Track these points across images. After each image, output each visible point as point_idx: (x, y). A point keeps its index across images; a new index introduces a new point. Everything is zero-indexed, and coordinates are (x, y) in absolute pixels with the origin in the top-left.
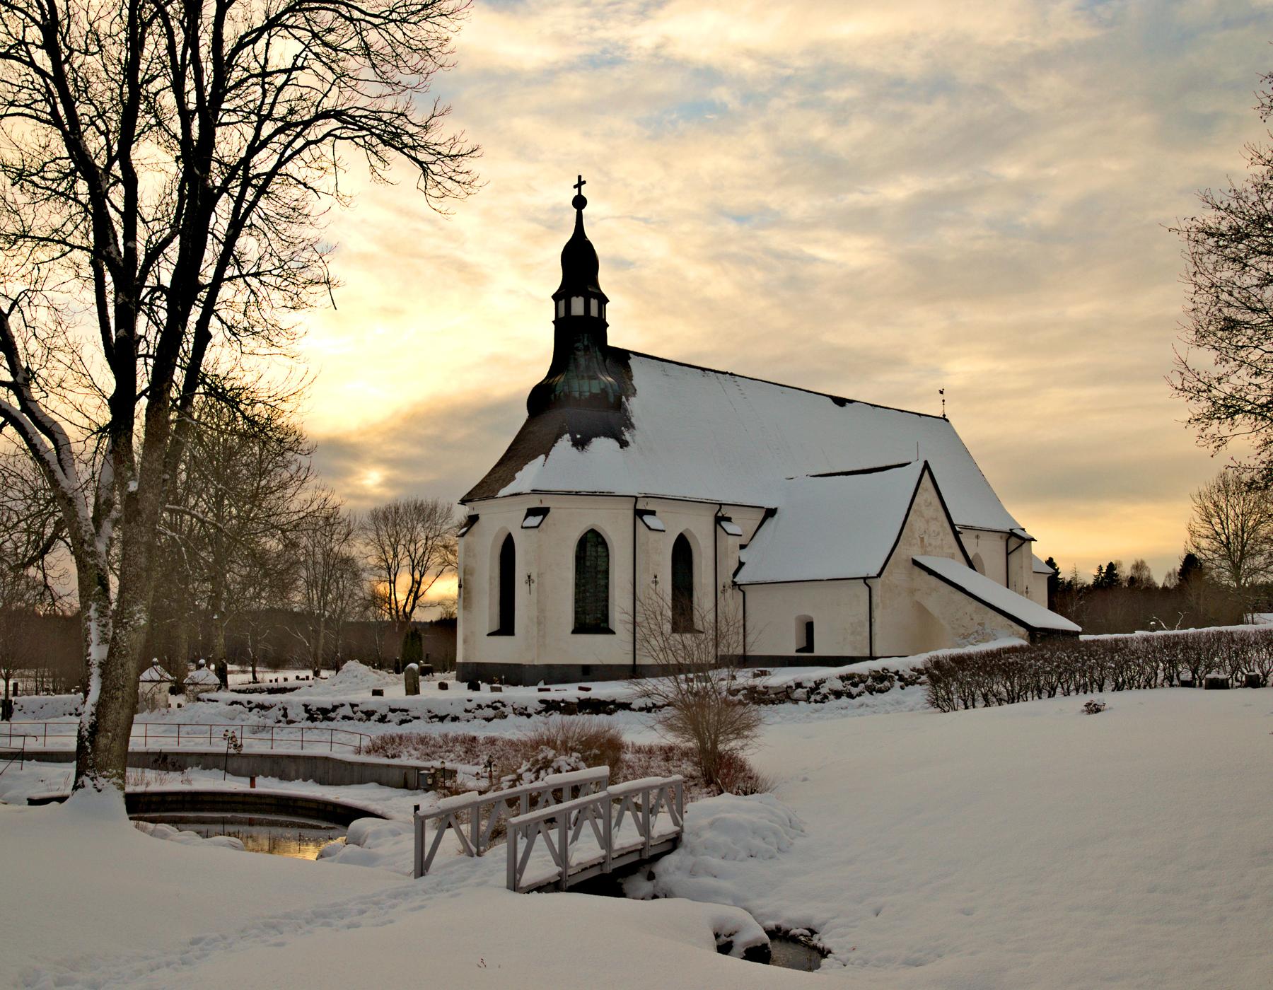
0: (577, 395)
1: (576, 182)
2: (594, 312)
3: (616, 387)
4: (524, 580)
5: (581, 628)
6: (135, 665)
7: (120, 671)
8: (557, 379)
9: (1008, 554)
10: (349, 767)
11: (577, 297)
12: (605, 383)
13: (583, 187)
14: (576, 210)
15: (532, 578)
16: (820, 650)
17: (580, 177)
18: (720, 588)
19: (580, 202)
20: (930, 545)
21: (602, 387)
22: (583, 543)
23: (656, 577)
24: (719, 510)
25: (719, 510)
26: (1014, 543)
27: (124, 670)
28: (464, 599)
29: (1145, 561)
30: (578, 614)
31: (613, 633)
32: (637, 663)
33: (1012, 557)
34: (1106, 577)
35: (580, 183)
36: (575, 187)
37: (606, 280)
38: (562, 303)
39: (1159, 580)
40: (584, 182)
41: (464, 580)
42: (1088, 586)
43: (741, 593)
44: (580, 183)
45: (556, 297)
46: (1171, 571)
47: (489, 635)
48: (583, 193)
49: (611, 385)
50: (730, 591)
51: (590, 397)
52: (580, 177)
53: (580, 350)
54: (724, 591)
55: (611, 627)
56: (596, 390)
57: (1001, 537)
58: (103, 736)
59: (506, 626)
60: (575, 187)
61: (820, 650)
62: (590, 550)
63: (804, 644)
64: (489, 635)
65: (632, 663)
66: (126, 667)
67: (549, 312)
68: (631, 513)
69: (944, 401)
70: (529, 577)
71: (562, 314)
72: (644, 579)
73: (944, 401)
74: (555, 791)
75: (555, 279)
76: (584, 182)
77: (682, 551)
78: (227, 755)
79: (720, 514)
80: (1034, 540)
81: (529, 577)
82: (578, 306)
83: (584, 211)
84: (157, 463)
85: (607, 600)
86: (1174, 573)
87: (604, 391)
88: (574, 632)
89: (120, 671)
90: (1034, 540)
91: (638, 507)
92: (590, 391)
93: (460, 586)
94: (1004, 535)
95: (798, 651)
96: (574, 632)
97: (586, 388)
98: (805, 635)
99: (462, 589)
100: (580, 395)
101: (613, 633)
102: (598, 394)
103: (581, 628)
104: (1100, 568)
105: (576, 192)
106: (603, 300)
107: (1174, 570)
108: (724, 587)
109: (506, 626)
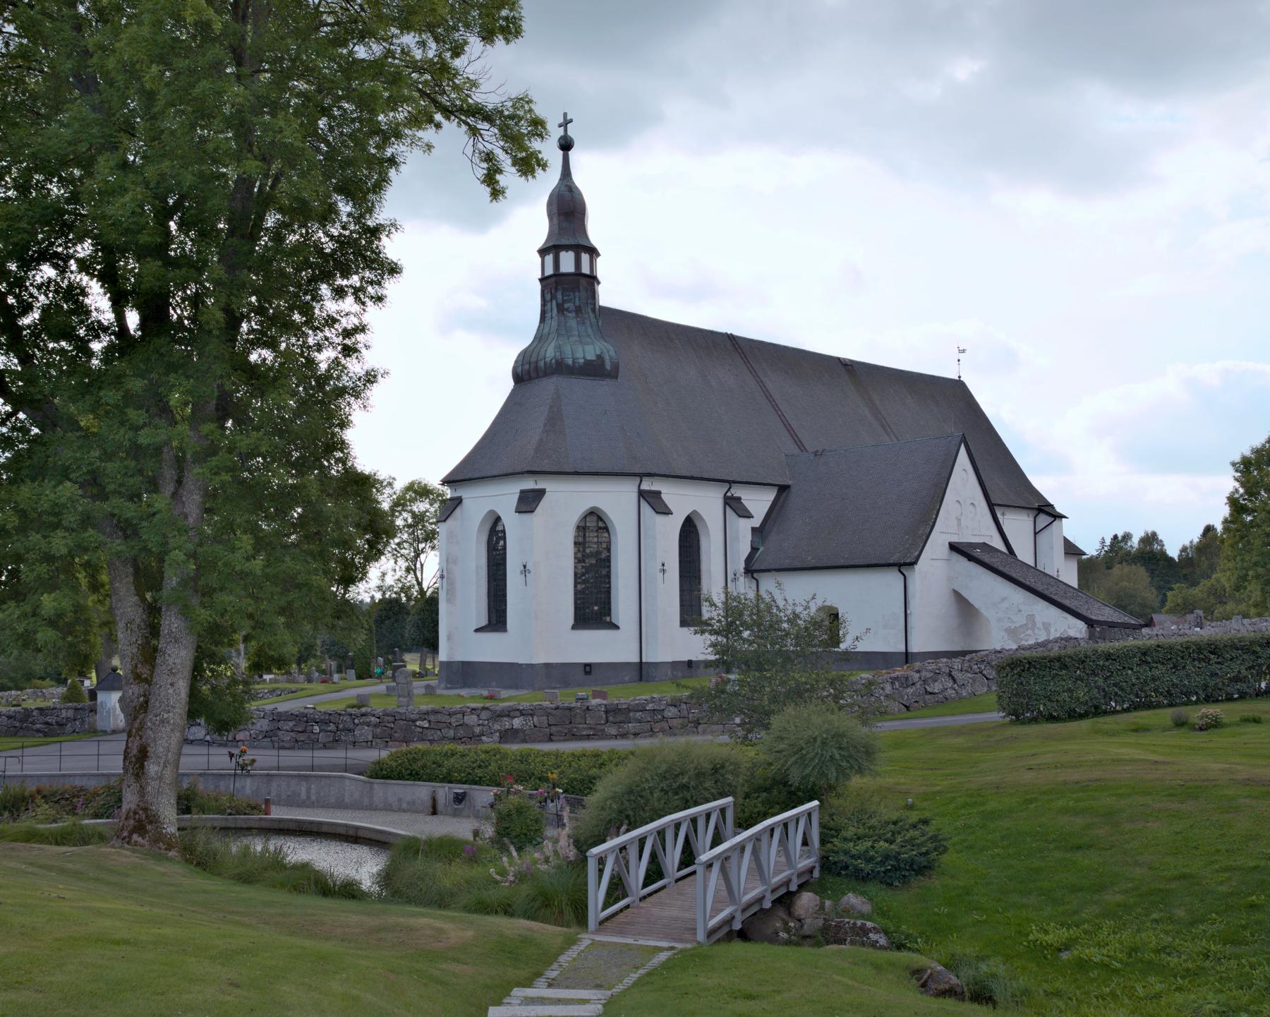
0: (570, 362)
1: (561, 120)
3: (612, 353)
4: (518, 571)
6: (185, 685)
7: (171, 691)
9: (1036, 534)
17: (565, 115)
20: (967, 527)
21: (598, 353)
22: (582, 529)
23: (663, 565)
27: (174, 691)
29: (1158, 533)
30: (578, 609)
31: (616, 627)
32: (644, 660)
33: (1041, 537)
34: (1111, 551)
36: (560, 126)
37: (596, 231)
38: (549, 259)
39: (1173, 552)
40: (571, 121)
41: (447, 569)
43: (755, 581)
45: (543, 252)
46: (1187, 544)
47: (477, 630)
48: (570, 133)
50: (742, 579)
51: (584, 363)
52: (565, 115)
53: (570, 312)
54: (735, 579)
58: (153, 763)
59: (497, 619)
60: (560, 126)
62: (592, 537)
64: (477, 630)
65: (637, 660)
66: (176, 686)
68: (635, 496)
69: (959, 360)
70: (525, 566)
72: (650, 567)
73: (959, 360)
74: (676, 824)
77: (690, 533)
79: (729, 494)
80: (1065, 517)
81: (525, 566)
82: (567, 262)
83: (570, 153)
85: (609, 592)
86: (1191, 547)
88: (574, 628)
89: (171, 691)
90: (1065, 517)
91: (642, 487)
92: (584, 358)
96: (574, 628)
100: (574, 362)
101: (616, 627)
102: (594, 361)
104: (1103, 541)
105: (561, 132)
107: (1191, 542)
108: (735, 575)
109: (497, 619)
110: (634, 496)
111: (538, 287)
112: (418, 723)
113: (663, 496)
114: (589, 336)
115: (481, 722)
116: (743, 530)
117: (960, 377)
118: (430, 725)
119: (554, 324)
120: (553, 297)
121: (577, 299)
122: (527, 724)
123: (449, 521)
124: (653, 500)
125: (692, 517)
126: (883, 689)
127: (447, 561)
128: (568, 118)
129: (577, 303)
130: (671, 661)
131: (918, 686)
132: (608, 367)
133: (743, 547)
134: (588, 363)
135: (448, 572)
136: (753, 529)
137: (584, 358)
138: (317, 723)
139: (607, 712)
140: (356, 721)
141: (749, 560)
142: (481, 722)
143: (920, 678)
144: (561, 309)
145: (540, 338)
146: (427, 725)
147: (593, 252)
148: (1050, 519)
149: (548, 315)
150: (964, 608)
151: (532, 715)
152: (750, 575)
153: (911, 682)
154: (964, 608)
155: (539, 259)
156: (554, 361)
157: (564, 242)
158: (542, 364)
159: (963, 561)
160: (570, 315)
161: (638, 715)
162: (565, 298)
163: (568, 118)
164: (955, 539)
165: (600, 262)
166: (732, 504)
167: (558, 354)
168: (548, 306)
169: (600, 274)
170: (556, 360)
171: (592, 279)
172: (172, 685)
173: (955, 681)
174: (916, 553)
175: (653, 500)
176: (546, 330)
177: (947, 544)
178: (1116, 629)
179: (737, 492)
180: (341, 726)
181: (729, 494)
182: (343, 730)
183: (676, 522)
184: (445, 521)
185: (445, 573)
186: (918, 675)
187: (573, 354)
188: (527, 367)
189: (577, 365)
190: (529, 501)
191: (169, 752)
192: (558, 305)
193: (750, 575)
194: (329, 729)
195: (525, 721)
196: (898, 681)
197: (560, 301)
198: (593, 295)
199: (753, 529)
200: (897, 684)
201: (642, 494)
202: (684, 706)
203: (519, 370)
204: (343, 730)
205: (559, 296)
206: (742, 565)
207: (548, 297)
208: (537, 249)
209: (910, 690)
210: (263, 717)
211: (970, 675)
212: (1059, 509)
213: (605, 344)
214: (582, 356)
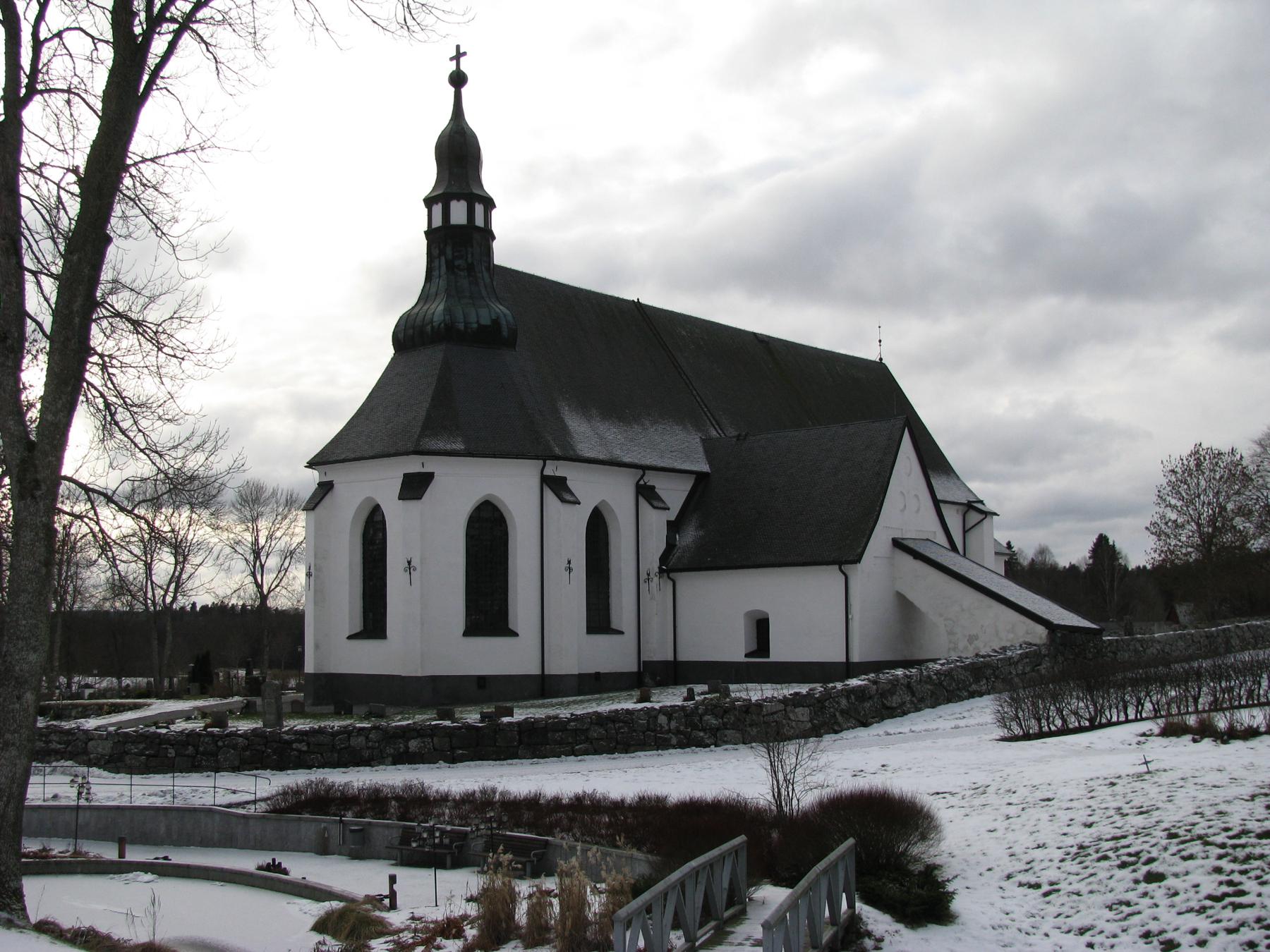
0: (461, 326)
1: (454, 54)
2: (479, 221)
3: (510, 318)
5: (472, 629)
8: (433, 306)
10: (242, 821)
11: (458, 200)
12: (496, 313)
13: (462, 60)
14: (453, 89)
15: (412, 564)
16: (780, 651)
17: (458, 47)
18: (643, 576)
19: (458, 80)
23: (569, 562)
24: (642, 478)
25: (642, 478)
26: (973, 517)
28: (316, 591)
31: (515, 634)
32: (546, 673)
35: (459, 56)
36: (452, 59)
37: (492, 179)
38: (438, 209)
40: (465, 54)
42: (1126, 568)
43: (670, 584)
44: (459, 56)
45: (429, 202)
47: (350, 638)
48: (462, 68)
49: (505, 315)
50: (656, 580)
52: (458, 47)
54: (648, 580)
55: (511, 626)
56: (485, 321)
57: (958, 511)
60: (452, 59)
61: (780, 651)
63: (754, 647)
64: (350, 638)
67: (417, 221)
69: (880, 341)
70: (409, 563)
71: (437, 222)
73: (880, 341)
75: (426, 176)
76: (465, 54)
77: (598, 527)
78: (78, 808)
79: (642, 482)
80: (995, 514)
81: (409, 563)
82: (459, 214)
83: (464, 90)
84: (62, 414)
87: (496, 322)
88: (466, 634)
91: (545, 473)
93: (309, 575)
94: (961, 508)
95: (746, 656)
96: (466, 634)
97: (473, 318)
98: (755, 635)
99: (312, 578)
100: (465, 327)
101: (515, 634)
103: (472, 629)
105: (452, 66)
106: (489, 204)
108: (648, 575)
110: (535, 482)
111: (424, 242)
112: (294, 746)
113: (568, 483)
114: (483, 298)
115: (370, 744)
116: (656, 523)
117: (881, 359)
118: (309, 747)
119: (442, 283)
120: (442, 253)
121: (469, 256)
122: (425, 747)
123: (317, 510)
124: (558, 486)
125: (602, 509)
126: (838, 703)
127: (315, 555)
128: (461, 51)
129: (470, 260)
130: (576, 672)
131: (875, 700)
132: (505, 333)
133: (655, 544)
134: (482, 328)
135: (316, 570)
136: (669, 522)
137: (478, 322)
138: (172, 745)
139: (520, 733)
140: (220, 743)
141: (664, 559)
142: (370, 744)
143: (877, 691)
144: (451, 267)
145: (424, 297)
146: (305, 748)
148: (981, 517)
149: (436, 273)
150: (906, 610)
151: (432, 736)
152: (665, 574)
153: (868, 696)
154: (906, 610)
155: (426, 211)
156: (443, 325)
157: (455, 190)
158: (429, 328)
159: (907, 559)
160: (462, 273)
161: (558, 735)
162: (456, 254)
163: (461, 51)
164: (898, 535)
165: (495, 215)
166: (646, 493)
167: (448, 317)
168: (436, 263)
169: (496, 227)
170: (445, 325)
171: (488, 235)
172: (19, 698)
173: (913, 694)
174: (859, 550)
175: (558, 486)
176: (433, 290)
177: (891, 540)
178: (1076, 634)
179: (652, 479)
180: (201, 749)
181: (642, 482)
182: (203, 754)
183: (584, 512)
184: (313, 509)
185: (312, 570)
186: (875, 687)
187: (465, 317)
188: (411, 331)
189: (469, 330)
190: (414, 487)
191: (14, 783)
192: (447, 262)
193: (665, 574)
194: (187, 752)
195: (424, 742)
196: (854, 694)
197: (450, 256)
198: (488, 252)
199: (669, 522)
200: (853, 697)
201: (546, 481)
202: (611, 725)
203: (401, 336)
204: (203, 754)
205: (449, 251)
206: (656, 564)
207: (436, 252)
208: (424, 197)
209: (867, 705)
210: (106, 739)
211: (929, 687)
212: (990, 505)
213: (501, 307)
214: (476, 320)
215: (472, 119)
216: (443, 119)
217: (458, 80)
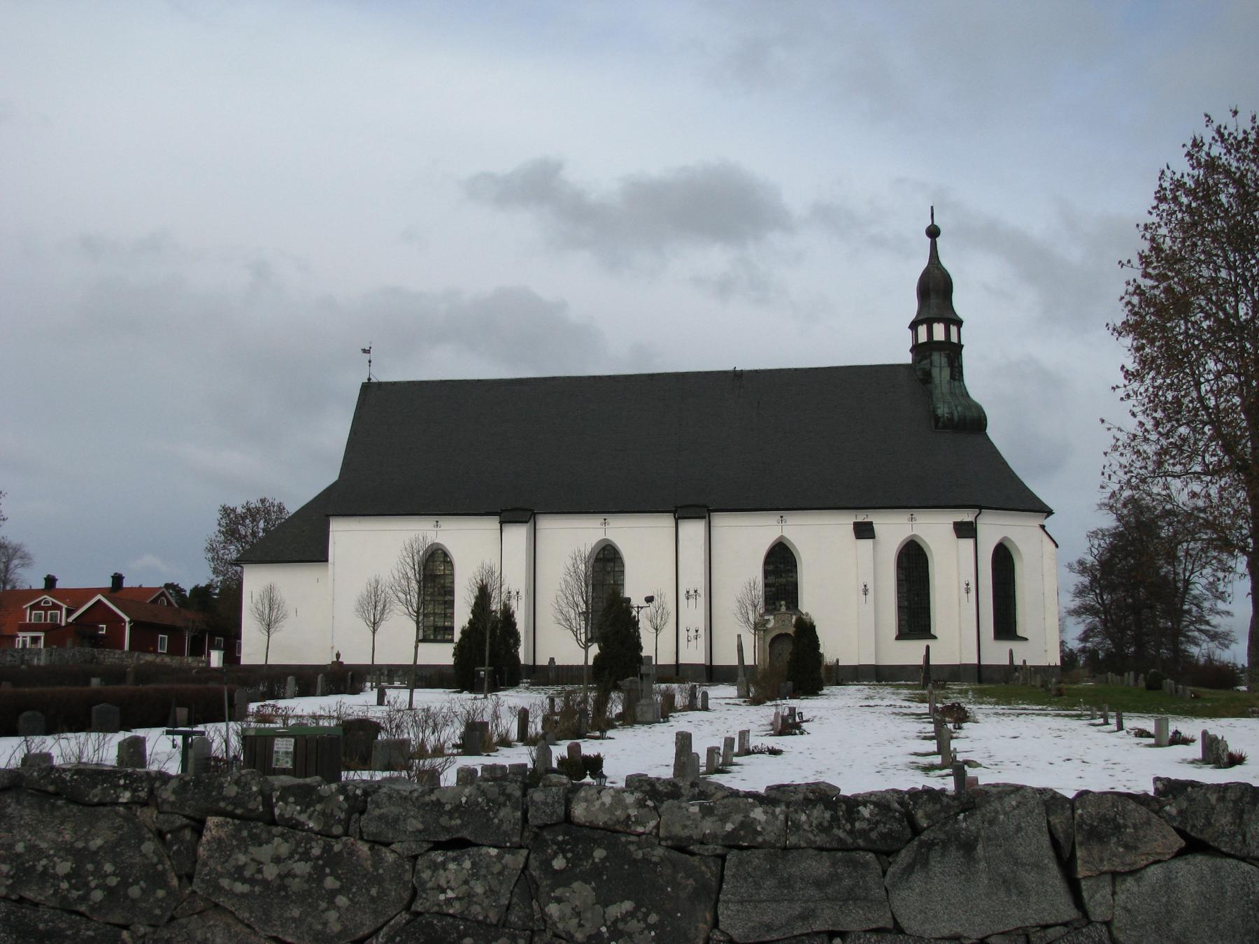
14: (930, 240)
19: (933, 232)
37: (960, 303)
75: (911, 308)
147: (959, 323)
215: (946, 262)
216: (922, 263)
217: (933, 232)
